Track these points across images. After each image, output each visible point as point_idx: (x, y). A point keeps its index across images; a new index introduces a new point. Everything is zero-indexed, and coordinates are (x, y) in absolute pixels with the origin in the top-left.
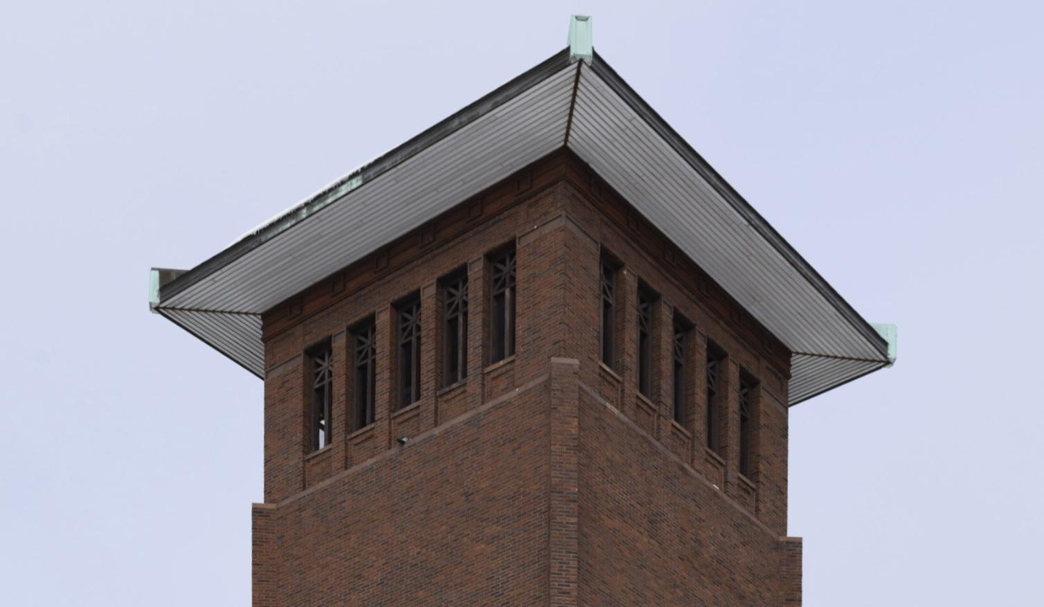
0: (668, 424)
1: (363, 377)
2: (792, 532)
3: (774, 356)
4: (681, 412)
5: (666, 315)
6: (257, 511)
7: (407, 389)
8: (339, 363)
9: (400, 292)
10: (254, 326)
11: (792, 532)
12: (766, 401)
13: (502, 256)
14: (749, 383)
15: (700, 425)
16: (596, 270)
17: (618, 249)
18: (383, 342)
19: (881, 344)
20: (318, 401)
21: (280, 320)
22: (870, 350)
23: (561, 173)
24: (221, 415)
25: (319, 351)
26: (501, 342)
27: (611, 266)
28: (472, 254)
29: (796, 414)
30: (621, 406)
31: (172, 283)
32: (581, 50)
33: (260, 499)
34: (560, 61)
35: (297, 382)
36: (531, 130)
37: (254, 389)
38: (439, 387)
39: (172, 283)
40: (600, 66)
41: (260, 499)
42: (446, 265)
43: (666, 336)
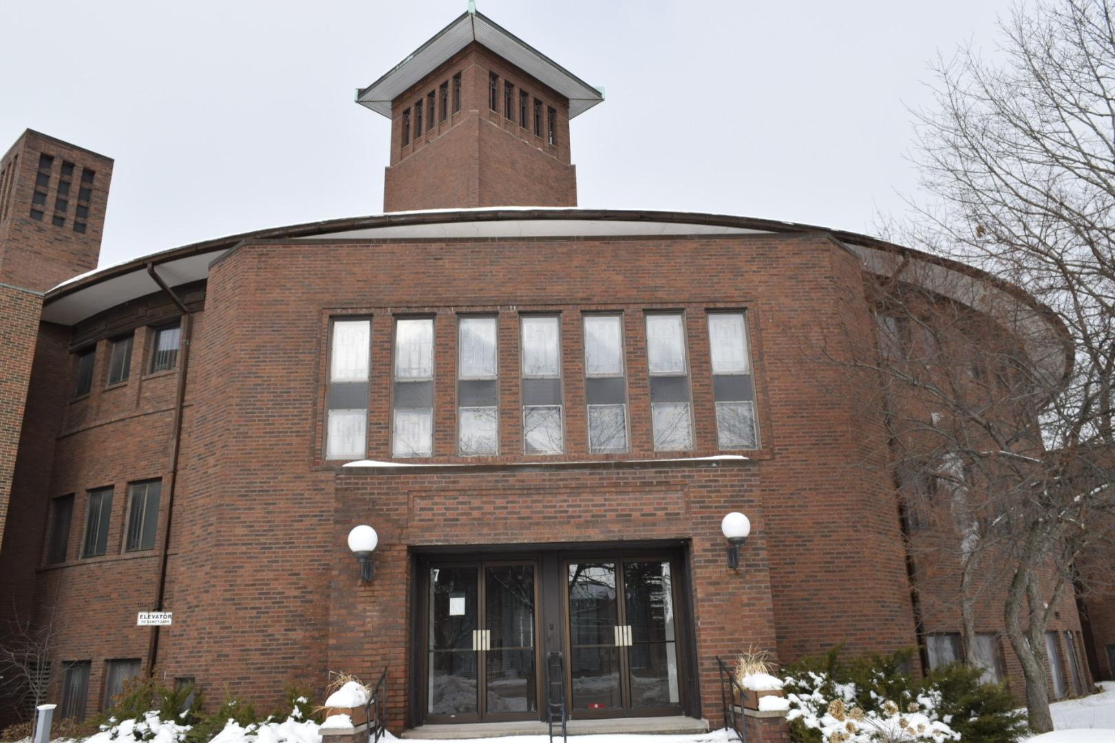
0: (518, 128)
1: (419, 118)
2: (572, 163)
3: (564, 101)
4: (524, 123)
5: (516, 91)
6: (387, 169)
7: (431, 124)
8: (412, 116)
9: (430, 91)
10: (389, 105)
11: (572, 163)
12: (559, 117)
13: (457, 77)
14: (552, 111)
15: (532, 127)
16: (487, 78)
17: (496, 71)
18: (424, 108)
19: (599, 94)
20: (406, 127)
21: (397, 101)
22: (595, 96)
23: (476, 48)
24: (380, 128)
25: (407, 112)
26: (457, 107)
27: (494, 77)
28: (449, 77)
29: (571, 122)
30: (498, 124)
31: (361, 93)
32: (472, 11)
33: (388, 165)
34: (466, 14)
35: (400, 123)
36: (462, 37)
37: (390, 121)
38: (143, 372)
39: (361, 93)
40: (478, 14)
41: (388, 165)
42: (442, 81)
43: (516, 99)
